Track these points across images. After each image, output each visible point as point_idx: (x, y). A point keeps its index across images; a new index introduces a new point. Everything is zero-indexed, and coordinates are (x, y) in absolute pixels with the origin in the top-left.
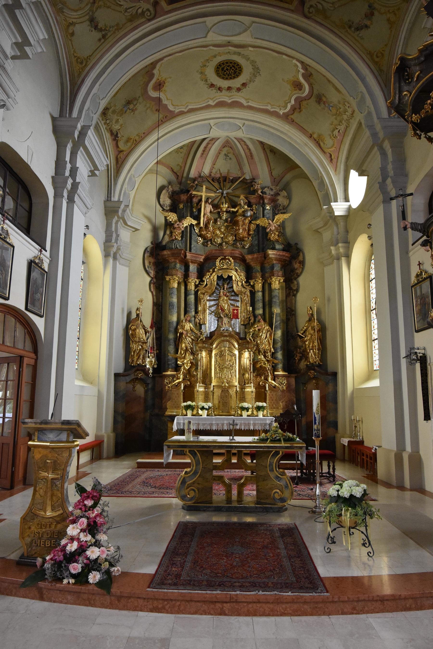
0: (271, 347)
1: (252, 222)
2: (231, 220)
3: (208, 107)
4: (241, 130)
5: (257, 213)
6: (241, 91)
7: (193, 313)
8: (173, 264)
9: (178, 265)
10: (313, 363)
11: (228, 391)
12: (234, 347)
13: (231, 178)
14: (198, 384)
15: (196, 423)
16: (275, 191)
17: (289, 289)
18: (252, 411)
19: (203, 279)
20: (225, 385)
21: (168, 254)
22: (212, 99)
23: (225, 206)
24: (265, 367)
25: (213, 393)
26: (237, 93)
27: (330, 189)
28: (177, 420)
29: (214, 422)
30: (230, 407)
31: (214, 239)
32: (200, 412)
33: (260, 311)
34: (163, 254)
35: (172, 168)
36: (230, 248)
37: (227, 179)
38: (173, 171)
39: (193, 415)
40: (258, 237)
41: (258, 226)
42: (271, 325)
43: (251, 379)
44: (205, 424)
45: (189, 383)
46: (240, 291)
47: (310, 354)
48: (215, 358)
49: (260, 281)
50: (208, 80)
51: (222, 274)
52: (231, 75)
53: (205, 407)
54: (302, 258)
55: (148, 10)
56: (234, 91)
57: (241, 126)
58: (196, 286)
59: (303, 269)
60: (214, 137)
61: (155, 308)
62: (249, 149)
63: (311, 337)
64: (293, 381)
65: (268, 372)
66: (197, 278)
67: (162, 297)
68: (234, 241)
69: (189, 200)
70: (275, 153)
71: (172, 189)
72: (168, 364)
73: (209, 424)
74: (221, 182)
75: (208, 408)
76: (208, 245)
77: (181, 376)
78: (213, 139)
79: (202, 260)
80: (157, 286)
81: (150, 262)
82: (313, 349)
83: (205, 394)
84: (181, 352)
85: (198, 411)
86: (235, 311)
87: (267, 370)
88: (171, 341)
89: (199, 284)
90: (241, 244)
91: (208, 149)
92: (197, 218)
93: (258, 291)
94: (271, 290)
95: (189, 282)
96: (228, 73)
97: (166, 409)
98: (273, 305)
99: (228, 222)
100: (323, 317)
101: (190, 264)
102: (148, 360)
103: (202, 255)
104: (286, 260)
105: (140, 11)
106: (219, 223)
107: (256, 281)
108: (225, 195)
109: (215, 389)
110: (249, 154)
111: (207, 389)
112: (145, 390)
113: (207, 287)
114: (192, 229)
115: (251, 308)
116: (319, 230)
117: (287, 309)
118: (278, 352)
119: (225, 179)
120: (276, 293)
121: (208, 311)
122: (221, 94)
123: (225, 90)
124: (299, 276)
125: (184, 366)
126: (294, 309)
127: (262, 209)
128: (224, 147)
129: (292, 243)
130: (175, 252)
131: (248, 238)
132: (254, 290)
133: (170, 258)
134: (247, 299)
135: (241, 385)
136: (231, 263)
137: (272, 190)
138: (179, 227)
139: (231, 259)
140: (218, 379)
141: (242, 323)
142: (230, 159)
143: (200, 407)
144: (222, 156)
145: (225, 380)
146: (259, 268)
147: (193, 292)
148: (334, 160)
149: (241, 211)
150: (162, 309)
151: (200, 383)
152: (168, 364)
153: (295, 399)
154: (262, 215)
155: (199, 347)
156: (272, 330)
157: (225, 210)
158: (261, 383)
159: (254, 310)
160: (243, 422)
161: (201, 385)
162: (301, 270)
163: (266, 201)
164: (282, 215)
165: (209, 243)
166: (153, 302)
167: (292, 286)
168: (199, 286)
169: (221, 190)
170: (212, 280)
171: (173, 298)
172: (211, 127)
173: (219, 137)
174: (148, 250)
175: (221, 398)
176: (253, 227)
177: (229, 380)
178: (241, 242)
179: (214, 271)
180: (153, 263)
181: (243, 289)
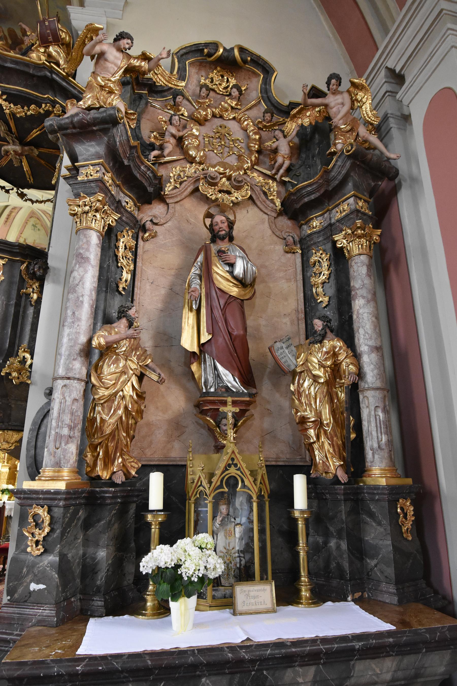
60: (16, 206)
78: (14, 208)
91: (11, 217)
142: (39, 230)
144: (29, 226)
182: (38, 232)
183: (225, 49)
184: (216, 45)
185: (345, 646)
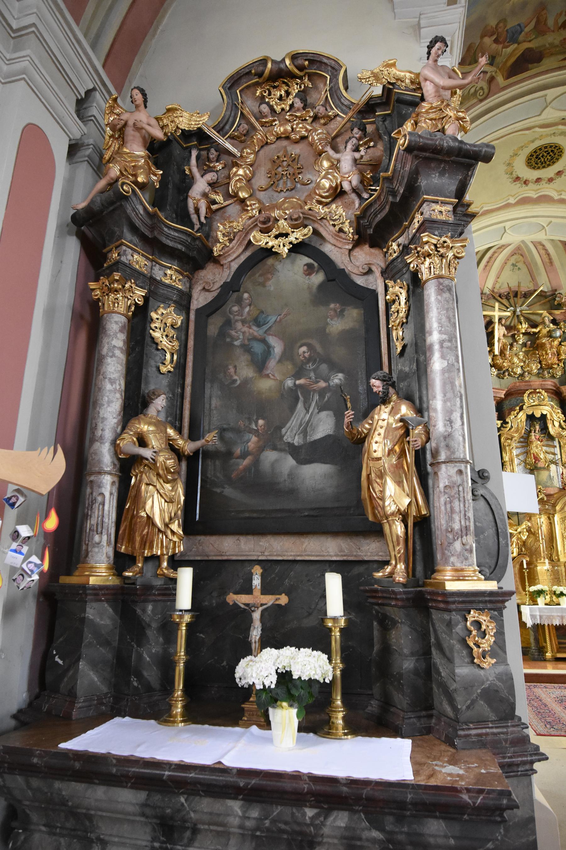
1: (562, 343)
3: (508, 206)
4: (544, 231)
6: (554, 181)
13: (523, 293)
15: (558, 616)
19: (507, 420)
22: (513, 196)
23: (524, 327)
26: (547, 185)
31: (513, 369)
36: (533, 378)
37: (519, 293)
39: (546, 604)
50: (514, 173)
52: (545, 163)
55: (482, 88)
56: (543, 182)
57: (545, 226)
60: (504, 244)
62: (549, 255)
66: (498, 420)
68: (538, 370)
76: (505, 376)
78: (503, 246)
79: (503, 396)
89: (502, 426)
91: (493, 259)
96: (543, 160)
99: (528, 347)
105: (473, 90)
106: (515, 349)
108: (518, 313)
113: (512, 430)
121: (516, 461)
122: (527, 188)
123: (532, 182)
131: (558, 365)
139: (543, 392)
142: (519, 269)
144: (508, 266)
149: (545, 331)
151: (544, 558)
165: (507, 374)
168: (502, 429)
170: (519, 421)
172: (505, 230)
173: (510, 243)
178: (548, 370)
179: (521, 409)
182: (517, 272)
183: (273, 62)
184: (264, 61)
185: (149, 773)
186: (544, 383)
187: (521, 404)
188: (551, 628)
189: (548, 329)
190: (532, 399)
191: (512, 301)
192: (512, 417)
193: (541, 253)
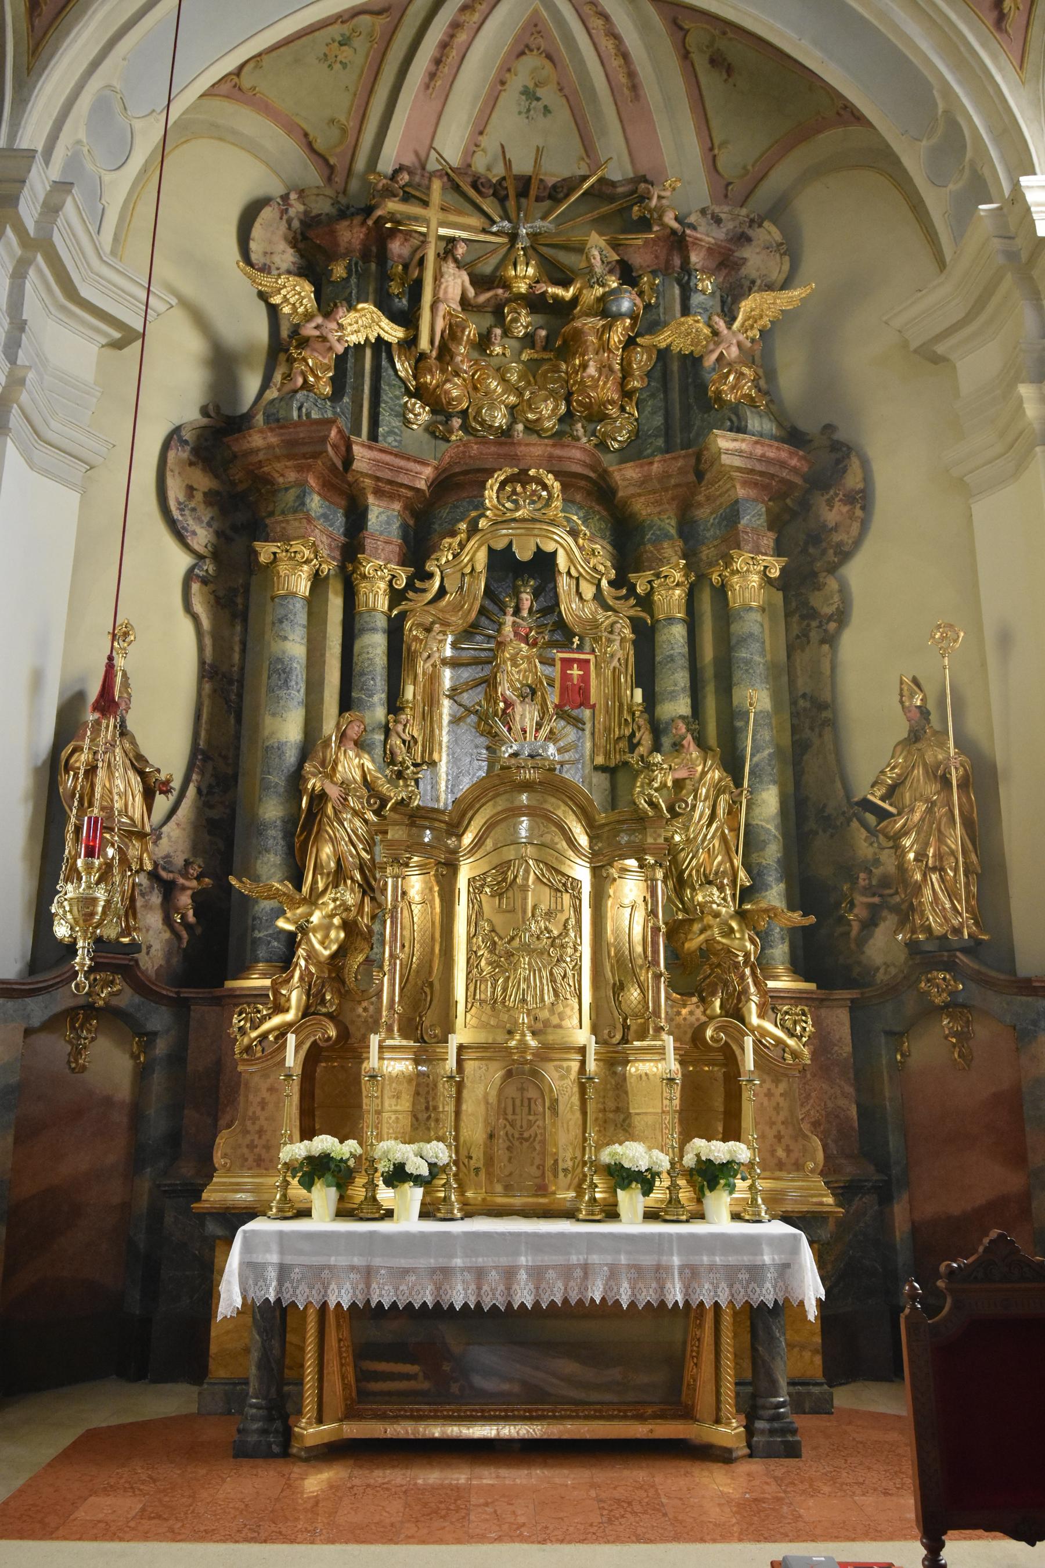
0: (737, 862)
2: (547, 337)
5: (657, 305)
7: (380, 713)
8: (292, 493)
9: (315, 503)
10: (944, 937)
11: (535, 1073)
12: (572, 843)
14: (374, 1040)
15: (353, 1268)
16: (730, 225)
17: (803, 617)
18: (673, 1188)
20: (523, 1042)
21: (270, 447)
24: (728, 951)
25: (460, 1087)
27: (994, 153)
28: (246, 1248)
29: (458, 1262)
30: (550, 1162)
32: (385, 1195)
33: (677, 707)
34: (245, 446)
35: (306, 135)
38: (310, 147)
40: (666, 400)
41: (663, 355)
42: (733, 765)
43: (656, 1013)
44: (406, 1272)
45: (332, 1033)
46: (588, 621)
47: (928, 892)
48: (470, 901)
49: (678, 576)
51: (510, 544)
53: (409, 1169)
54: (860, 475)
58: (396, 596)
59: (865, 526)
61: (207, 687)
62: (625, 56)
63: (930, 811)
64: (840, 1022)
65: (742, 977)
66: (403, 563)
67: (244, 644)
69: (374, 249)
70: (729, 70)
71: (301, 208)
72: (255, 942)
73: (433, 1271)
74: (507, 196)
75: (425, 1171)
76: (451, 432)
77: (295, 997)
80: (221, 594)
81: (190, 490)
82: (941, 870)
83: (417, 1093)
84: (314, 882)
85: (371, 1186)
86: (575, 672)
87: (736, 965)
88: (271, 832)
89: (410, 585)
90: (594, 434)
91: (454, 54)
92: (408, 319)
93: (670, 620)
94: (725, 614)
95: (364, 577)
97: (207, 1171)
98: (738, 675)
100: (974, 727)
101: (371, 499)
102: (70, 890)
103: (424, 463)
104: (790, 485)
106: (498, 350)
107: (658, 576)
109: (470, 1066)
110: (624, 80)
111: (428, 1061)
112: (137, 1065)
113: (443, 603)
114: (384, 363)
115: (638, 693)
116: (940, 349)
117: (794, 703)
118: (766, 887)
119: (524, 185)
120: (753, 624)
124: (845, 555)
125: (309, 941)
126: (826, 696)
127: (677, 291)
128: (522, 53)
129: (809, 426)
130: (302, 433)
131: (623, 409)
132: (652, 617)
133: (278, 466)
134: (620, 654)
135: (606, 1043)
136: (550, 494)
137: (718, 221)
138: (324, 339)
139: (550, 479)
140: (488, 1008)
141: (600, 760)
142: (546, 110)
143: (383, 1167)
144: (511, 99)
145: (523, 1019)
146: (670, 524)
147: (381, 622)
148: (1015, 20)
150: (240, 696)
151: (390, 1029)
152: (255, 942)
153: (853, 1111)
154: (678, 307)
155: (390, 845)
156: (738, 784)
157: (523, 287)
158: (709, 1033)
159: (651, 700)
160: (623, 1259)
161: (397, 1041)
162: (855, 527)
163: (695, 258)
164: (769, 296)
165: (456, 422)
166: (202, 662)
167: (816, 600)
168: (411, 594)
169: (506, 223)
170: (468, 570)
171: (285, 638)
174: (187, 435)
175: (502, 1112)
176: (641, 360)
177: (544, 1014)
178: (590, 427)
180: (205, 494)
181: (600, 615)
186: (558, 452)
187: (474, 514)
188: (331, 1320)
189: (599, 291)
190: (509, 499)
191: (511, 204)
192: (447, 556)
193: (602, 49)
